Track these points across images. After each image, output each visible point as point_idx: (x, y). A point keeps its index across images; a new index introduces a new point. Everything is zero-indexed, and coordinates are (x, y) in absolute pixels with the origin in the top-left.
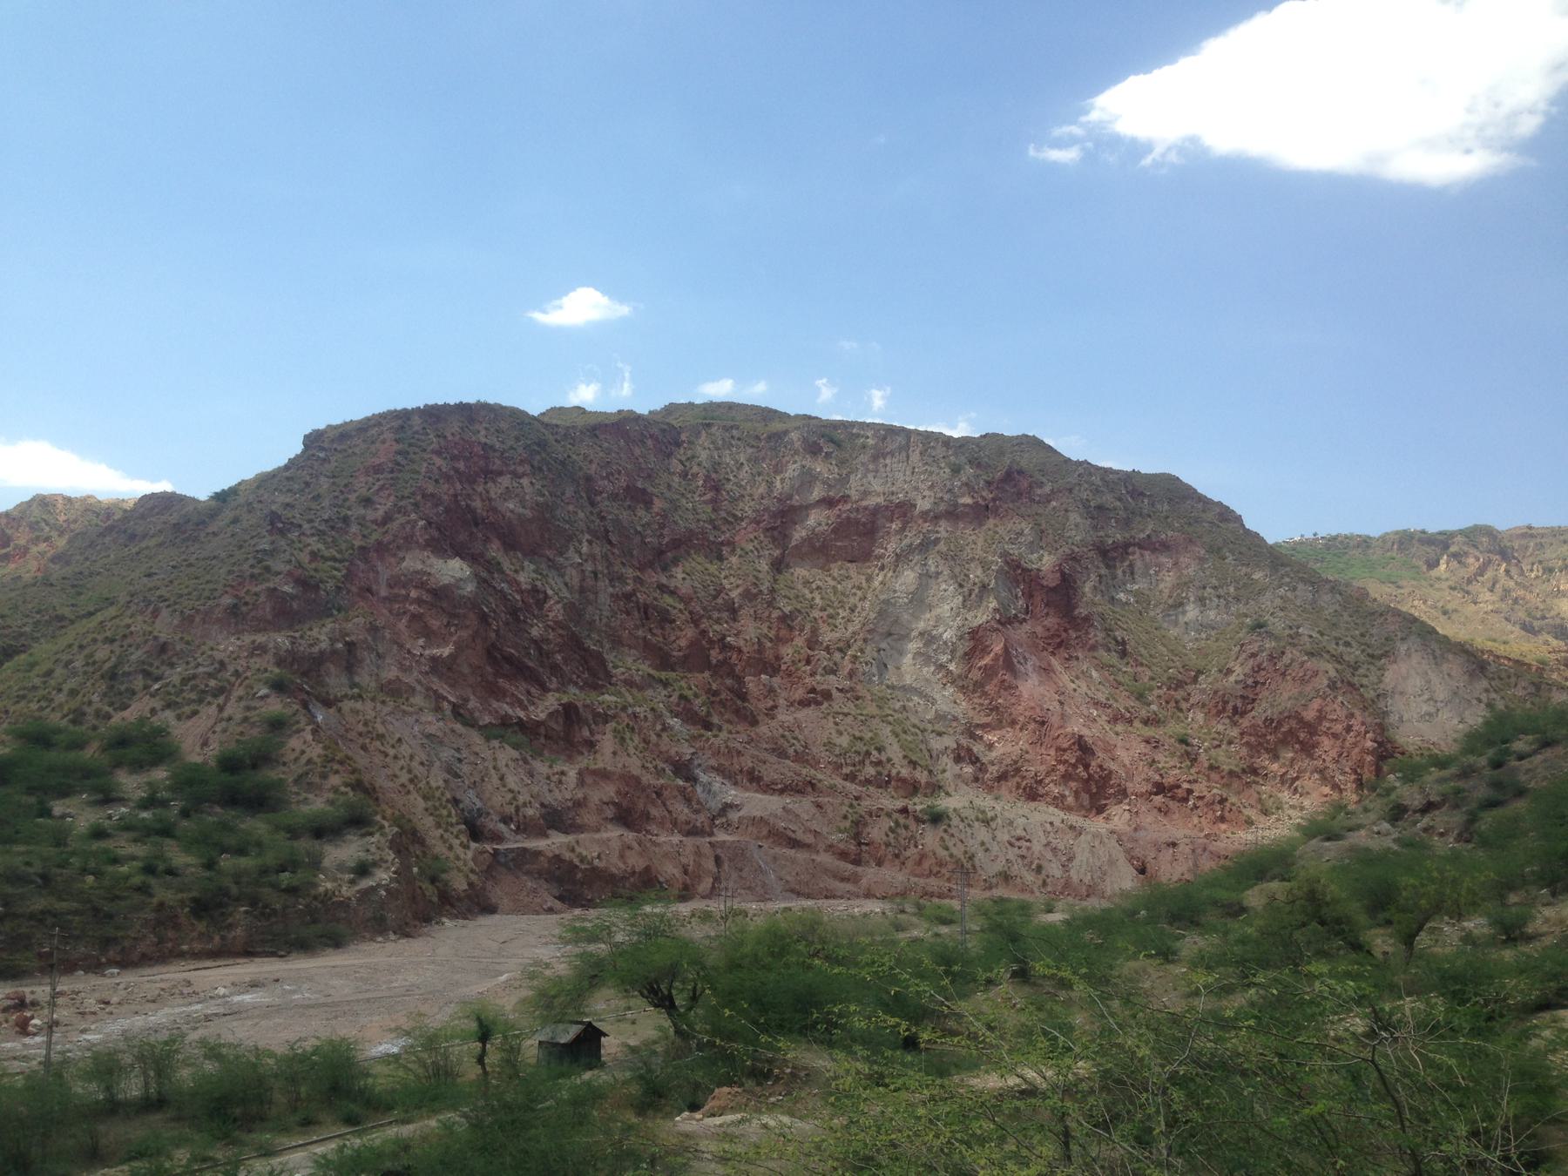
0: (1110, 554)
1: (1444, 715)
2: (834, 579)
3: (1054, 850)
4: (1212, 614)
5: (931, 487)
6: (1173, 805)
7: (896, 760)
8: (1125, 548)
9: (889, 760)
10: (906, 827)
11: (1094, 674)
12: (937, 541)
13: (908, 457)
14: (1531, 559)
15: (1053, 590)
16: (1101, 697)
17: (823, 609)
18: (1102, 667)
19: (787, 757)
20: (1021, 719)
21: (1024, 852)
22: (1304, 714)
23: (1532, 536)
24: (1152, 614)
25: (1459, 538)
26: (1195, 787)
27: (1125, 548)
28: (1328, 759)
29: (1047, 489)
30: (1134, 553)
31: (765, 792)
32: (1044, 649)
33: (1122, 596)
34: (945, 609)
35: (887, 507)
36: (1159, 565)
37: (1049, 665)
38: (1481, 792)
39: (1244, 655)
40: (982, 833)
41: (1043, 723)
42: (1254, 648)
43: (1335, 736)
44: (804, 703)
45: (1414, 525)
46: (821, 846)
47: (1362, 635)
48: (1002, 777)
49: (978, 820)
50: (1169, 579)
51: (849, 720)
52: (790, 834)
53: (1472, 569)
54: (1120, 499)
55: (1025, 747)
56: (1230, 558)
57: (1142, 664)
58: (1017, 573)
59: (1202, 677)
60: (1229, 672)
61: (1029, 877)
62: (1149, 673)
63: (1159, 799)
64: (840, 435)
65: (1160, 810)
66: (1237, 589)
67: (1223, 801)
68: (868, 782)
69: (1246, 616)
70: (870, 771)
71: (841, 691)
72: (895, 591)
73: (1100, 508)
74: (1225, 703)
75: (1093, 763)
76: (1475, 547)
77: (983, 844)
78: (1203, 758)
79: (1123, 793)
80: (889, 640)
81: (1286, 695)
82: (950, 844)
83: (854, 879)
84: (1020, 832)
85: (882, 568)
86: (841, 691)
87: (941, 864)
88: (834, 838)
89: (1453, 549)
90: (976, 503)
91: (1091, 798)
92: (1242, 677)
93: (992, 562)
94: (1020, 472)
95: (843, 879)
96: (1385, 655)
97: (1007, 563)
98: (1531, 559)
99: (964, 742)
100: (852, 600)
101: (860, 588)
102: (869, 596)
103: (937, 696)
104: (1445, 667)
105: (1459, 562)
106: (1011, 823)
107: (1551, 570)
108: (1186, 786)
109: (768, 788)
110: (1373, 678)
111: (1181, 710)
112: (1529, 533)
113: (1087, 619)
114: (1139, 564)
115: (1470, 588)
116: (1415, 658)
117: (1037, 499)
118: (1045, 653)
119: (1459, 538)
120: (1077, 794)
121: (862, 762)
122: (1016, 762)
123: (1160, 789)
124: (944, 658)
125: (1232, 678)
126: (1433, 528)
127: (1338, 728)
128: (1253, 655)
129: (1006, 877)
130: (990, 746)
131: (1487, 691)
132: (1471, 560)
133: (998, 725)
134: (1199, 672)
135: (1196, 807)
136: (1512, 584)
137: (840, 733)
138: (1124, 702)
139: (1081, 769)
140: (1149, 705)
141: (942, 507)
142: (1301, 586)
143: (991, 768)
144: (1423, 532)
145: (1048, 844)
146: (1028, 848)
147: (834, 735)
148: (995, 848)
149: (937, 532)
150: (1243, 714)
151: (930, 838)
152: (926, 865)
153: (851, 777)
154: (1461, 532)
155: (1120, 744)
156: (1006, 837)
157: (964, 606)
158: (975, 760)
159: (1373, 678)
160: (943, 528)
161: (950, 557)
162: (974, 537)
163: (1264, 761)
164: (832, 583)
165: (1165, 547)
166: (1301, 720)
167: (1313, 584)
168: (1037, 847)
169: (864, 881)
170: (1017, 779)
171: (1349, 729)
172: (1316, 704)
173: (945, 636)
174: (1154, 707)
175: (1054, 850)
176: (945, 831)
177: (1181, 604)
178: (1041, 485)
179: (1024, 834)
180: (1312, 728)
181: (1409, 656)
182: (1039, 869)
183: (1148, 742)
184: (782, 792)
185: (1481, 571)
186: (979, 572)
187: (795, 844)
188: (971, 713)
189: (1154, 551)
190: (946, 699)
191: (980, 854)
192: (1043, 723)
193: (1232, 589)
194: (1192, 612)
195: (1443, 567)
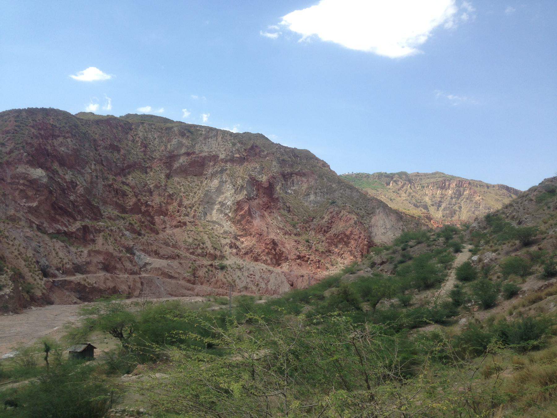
1: (389, 233)
2: (189, 182)
3: (263, 279)
4: (319, 198)
5: (225, 150)
6: (303, 263)
7: (209, 247)
9: (207, 247)
10: (212, 271)
14: (418, 183)
15: (265, 188)
17: (184, 193)
18: (281, 215)
19: (170, 246)
21: (252, 279)
23: (419, 176)
24: (299, 197)
25: (396, 176)
26: (311, 257)
27: (290, 175)
30: (294, 177)
31: (160, 258)
32: (262, 209)
33: (289, 191)
34: (228, 194)
36: (302, 181)
37: (264, 214)
38: (398, 258)
39: (328, 213)
40: (239, 273)
41: (261, 235)
42: (332, 210)
43: (355, 240)
44: (176, 227)
45: (383, 171)
46: (181, 278)
47: (365, 207)
48: (246, 253)
49: (237, 268)
50: (305, 186)
51: (193, 233)
52: (169, 273)
54: (290, 158)
55: (255, 243)
57: (295, 215)
59: (315, 220)
60: (324, 218)
61: (254, 288)
62: (297, 218)
63: (298, 261)
64: (192, 129)
67: (319, 261)
68: (199, 255)
70: (200, 251)
71: (190, 222)
72: (211, 187)
73: (283, 160)
74: (322, 228)
75: (277, 249)
77: (238, 276)
78: (314, 247)
79: (287, 259)
80: (208, 204)
81: (341, 226)
82: (227, 277)
83: (192, 289)
84: (251, 272)
85: (206, 179)
86: (190, 222)
88: (186, 275)
89: (394, 179)
90: (241, 157)
92: (327, 220)
94: (256, 146)
95: (188, 290)
96: (372, 213)
97: (251, 178)
98: (418, 183)
99: (233, 241)
100: (195, 190)
101: (198, 185)
103: (224, 225)
104: (390, 218)
105: (396, 183)
107: (424, 187)
108: (307, 256)
109: (162, 257)
110: (368, 221)
112: (418, 175)
113: (277, 199)
114: (295, 180)
115: (399, 192)
117: (262, 156)
118: (263, 210)
119: (396, 176)
120: (271, 259)
121: (197, 248)
122: (251, 248)
123: (299, 257)
124: (227, 211)
125: (324, 220)
126: (388, 172)
127: (356, 237)
128: (331, 213)
129: (246, 288)
130: (242, 243)
131: (402, 225)
132: (400, 183)
134: (314, 218)
135: (310, 264)
136: (412, 191)
137: (189, 237)
138: (289, 228)
139: (273, 251)
141: (229, 158)
142: (347, 190)
143: (242, 250)
145: (261, 277)
146: (254, 278)
147: (187, 238)
148: (243, 278)
149: (227, 166)
150: (327, 232)
151: (220, 275)
152: (218, 284)
153: (192, 253)
154: (397, 174)
155: (286, 242)
156: (247, 274)
158: (237, 247)
159: (368, 221)
160: (229, 165)
161: (231, 176)
162: (239, 169)
164: (188, 183)
165: (304, 175)
166: (345, 234)
167: (351, 189)
168: (257, 277)
169: (196, 290)
170: (251, 254)
171: (360, 237)
172: (350, 229)
173: (228, 204)
174: (298, 230)
175: (263, 279)
176: (226, 272)
177: (309, 195)
179: (253, 273)
181: (379, 213)
182: (258, 285)
183: (296, 241)
184: (167, 258)
185: (402, 187)
186: (241, 181)
187: (171, 277)
188: (236, 231)
189: (301, 176)
190: (228, 226)
191: (238, 280)
192: (261, 235)
193: (325, 190)
194: (312, 197)
195: (391, 185)
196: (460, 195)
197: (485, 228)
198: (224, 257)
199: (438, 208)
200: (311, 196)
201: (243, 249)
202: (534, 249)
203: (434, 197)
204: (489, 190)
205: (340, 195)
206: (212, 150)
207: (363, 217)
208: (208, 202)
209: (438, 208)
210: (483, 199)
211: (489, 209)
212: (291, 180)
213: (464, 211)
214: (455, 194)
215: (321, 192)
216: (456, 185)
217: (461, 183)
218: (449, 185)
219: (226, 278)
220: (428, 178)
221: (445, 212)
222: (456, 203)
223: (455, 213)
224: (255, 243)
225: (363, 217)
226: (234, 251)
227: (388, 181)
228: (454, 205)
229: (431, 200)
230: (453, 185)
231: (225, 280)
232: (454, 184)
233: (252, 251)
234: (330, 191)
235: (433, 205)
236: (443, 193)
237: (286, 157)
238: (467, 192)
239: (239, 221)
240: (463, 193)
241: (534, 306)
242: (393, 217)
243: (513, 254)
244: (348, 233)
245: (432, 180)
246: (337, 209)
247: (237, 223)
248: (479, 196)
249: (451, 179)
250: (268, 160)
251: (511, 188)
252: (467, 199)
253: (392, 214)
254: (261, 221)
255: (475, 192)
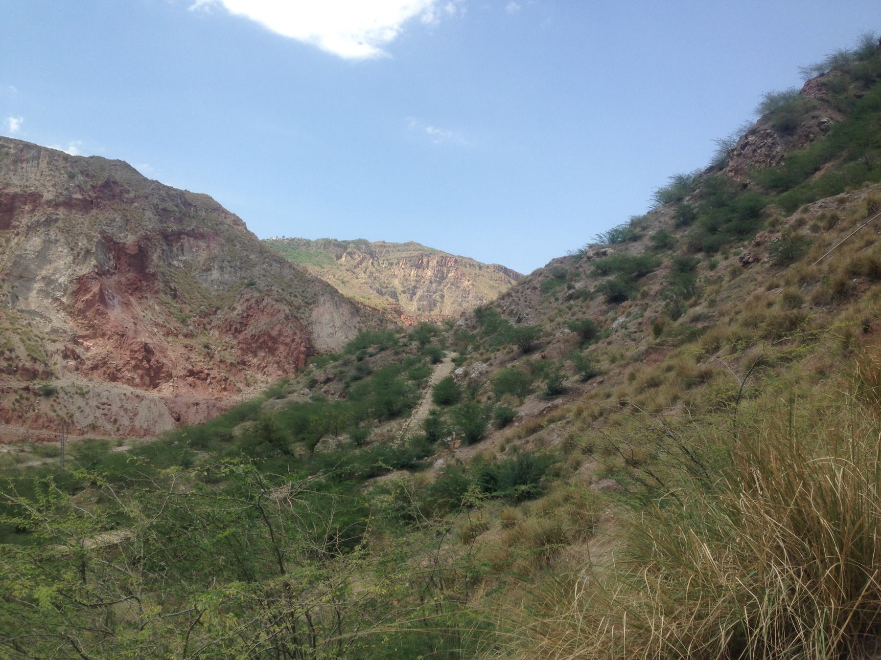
0: (169, 238)
1: (339, 334)
3: (126, 410)
4: (227, 276)
6: (198, 382)
7: (22, 357)
8: (179, 235)
9: (17, 357)
10: (27, 399)
11: (157, 307)
12: (57, 220)
13: (38, 164)
16: (160, 321)
18: (161, 303)
20: (109, 333)
21: (106, 411)
22: (272, 332)
23: (385, 246)
24: (193, 274)
25: (352, 245)
27: (179, 235)
28: (282, 356)
29: (132, 195)
30: (184, 238)
33: (175, 263)
35: (22, 195)
36: (198, 247)
39: (242, 300)
40: (80, 402)
41: (123, 336)
42: (247, 296)
43: (286, 344)
45: (332, 237)
47: (303, 292)
48: (95, 368)
49: (77, 393)
50: (203, 256)
53: (357, 261)
54: (177, 206)
55: (112, 349)
56: (238, 246)
57: (185, 303)
58: (110, 245)
59: (219, 311)
60: (234, 309)
61: (109, 427)
62: (189, 308)
65: (191, 385)
66: (241, 263)
67: (226, 379)
69: (245, 278)
72: (26, 250)
73: (164, 210)
74: (231, 326)
76: (359, 250)
77: (79, 408)
80: (21, 281)
81: (263, 322)
84: (104, 400)
85: (17, 234)
87: (51, 421)
89: (349, 250)
90: (85, 199)
91: (150, 380)
92: (240, 312)
93: (94, 236)
94: (115, 183)
96: (314, 302)
97: (104, 238)
102: (7, 252)
103: (53, 318)
104: (341, 310)
105: (351, 257)
106: (99, 395)
108: (206, 371)
111: (206, 329)
112: (383, 245)
113: (153, 275)
114: (186, 245)
116: (328, 304)
117: (125, 200)
120: (142, 377)
123: (191, 373)
125: (236, 312)
127: (288, 340)
128: (248, 300)
130: (88, 349)
131: (359, 322)
132: (356, 256)
133: (94, 336)
134: (218, 308)
135: (211, 383)
138: (174, 324)
139: (145, 362)
140: (188, 326)
141: (61, 199)
142: (274, 264)
143: (87, 362)
144: (336, 240)
146: (109, 410)
148: (87, 410)
149: (57, 214)
151: (44, 406)
152: (40, 422)
154: (353, 242)
155: (170, 348)
157: (74, 263)
158: (76, 357)
159: (307, 315)
160: (62, 212)
161: (66, 231)
162: (82, 220)
163: (249, 358)
165: (202, 236)
166: (270, 336)
167: (280, 263)
168: (115, 408)
170: (105, 369)
171: (293, 341)
172: (277, 328)
173: (60, 281)
175: (126, 410)
177: (210, 270)
178: (128, 192)
180: (275, 340)
181: (324, 303)
185: (361, 263)
186: (85, 242)
188: (75, 329)
189: (196, 238)
191: (77, 414)
192: (123, 336)
193: (238, 263)
194: (215, 274)
195: (344, 259)
196: (443, 278)
197: (474, 328)
198: (52, 374)
199: (412, 297)
200: (213, 272)
201: (88, 359)
202: (536, 356)
203: (406, 280)
204: (482, 272)
205: (262, 272)
206: (28, 184)
207: (299, 308)
208: (21, 277)
209: (412, 297)
210: (473, 285)
211: (480, 300)
212: (179, 244)
213: (448, 301)
214: (436, 276)
215: (231, 267)
216: (437, 263)
217: (444, 260)
218: (428, 262)
219: (55, 411)
220: (399, 251)
221: (421, 303)
222: (436, 289)
223: (435, 305)
224: (112, 349)
225: (299, 308)
226: (72, 363)
227: (339, 253)
228: (434, 293)
229: (403, 284)
230: (434, 263)
231: (54, 414)
232: (435, 262)
233: (105, 363)
234: (246, 264)
235: (404, 292)
236: (420, 273)
237: (169, 205)
238: (453, 274)
239: (82, 312)
240: (447, 276)
241: (532, 438)
242: (345, 309)
243: (509, 365)
244: (274, 333)
245: (404, 254)
246: (257, 295)
247: (78, 315)
248: (469, 281)
249: (431, 254)
250: (136, 207)
251: (511, 271)
252: (452, 284)
253: (344, 305)
254: (123, 312)
255: (463, 275)
